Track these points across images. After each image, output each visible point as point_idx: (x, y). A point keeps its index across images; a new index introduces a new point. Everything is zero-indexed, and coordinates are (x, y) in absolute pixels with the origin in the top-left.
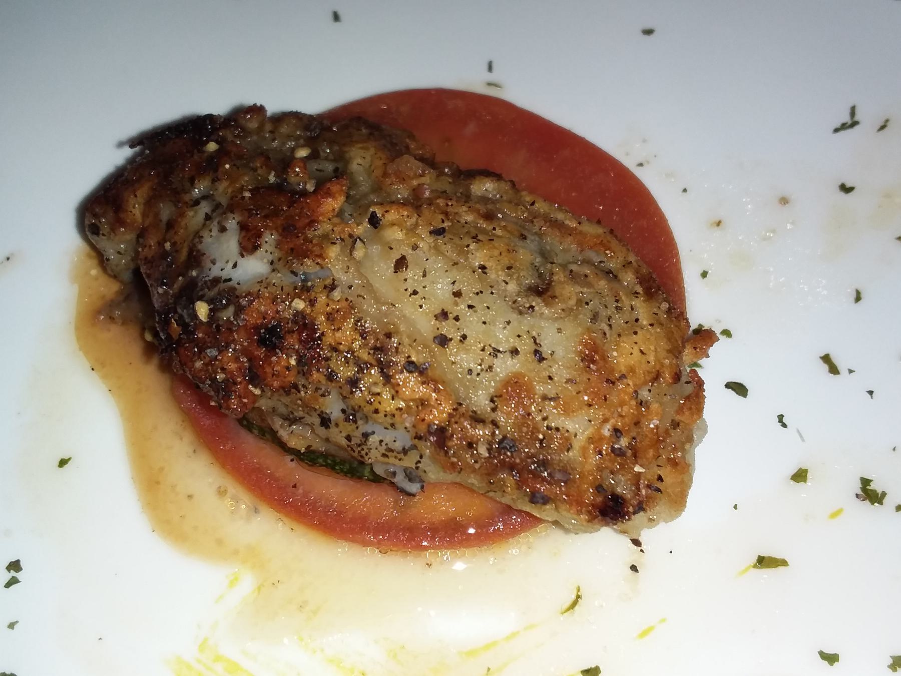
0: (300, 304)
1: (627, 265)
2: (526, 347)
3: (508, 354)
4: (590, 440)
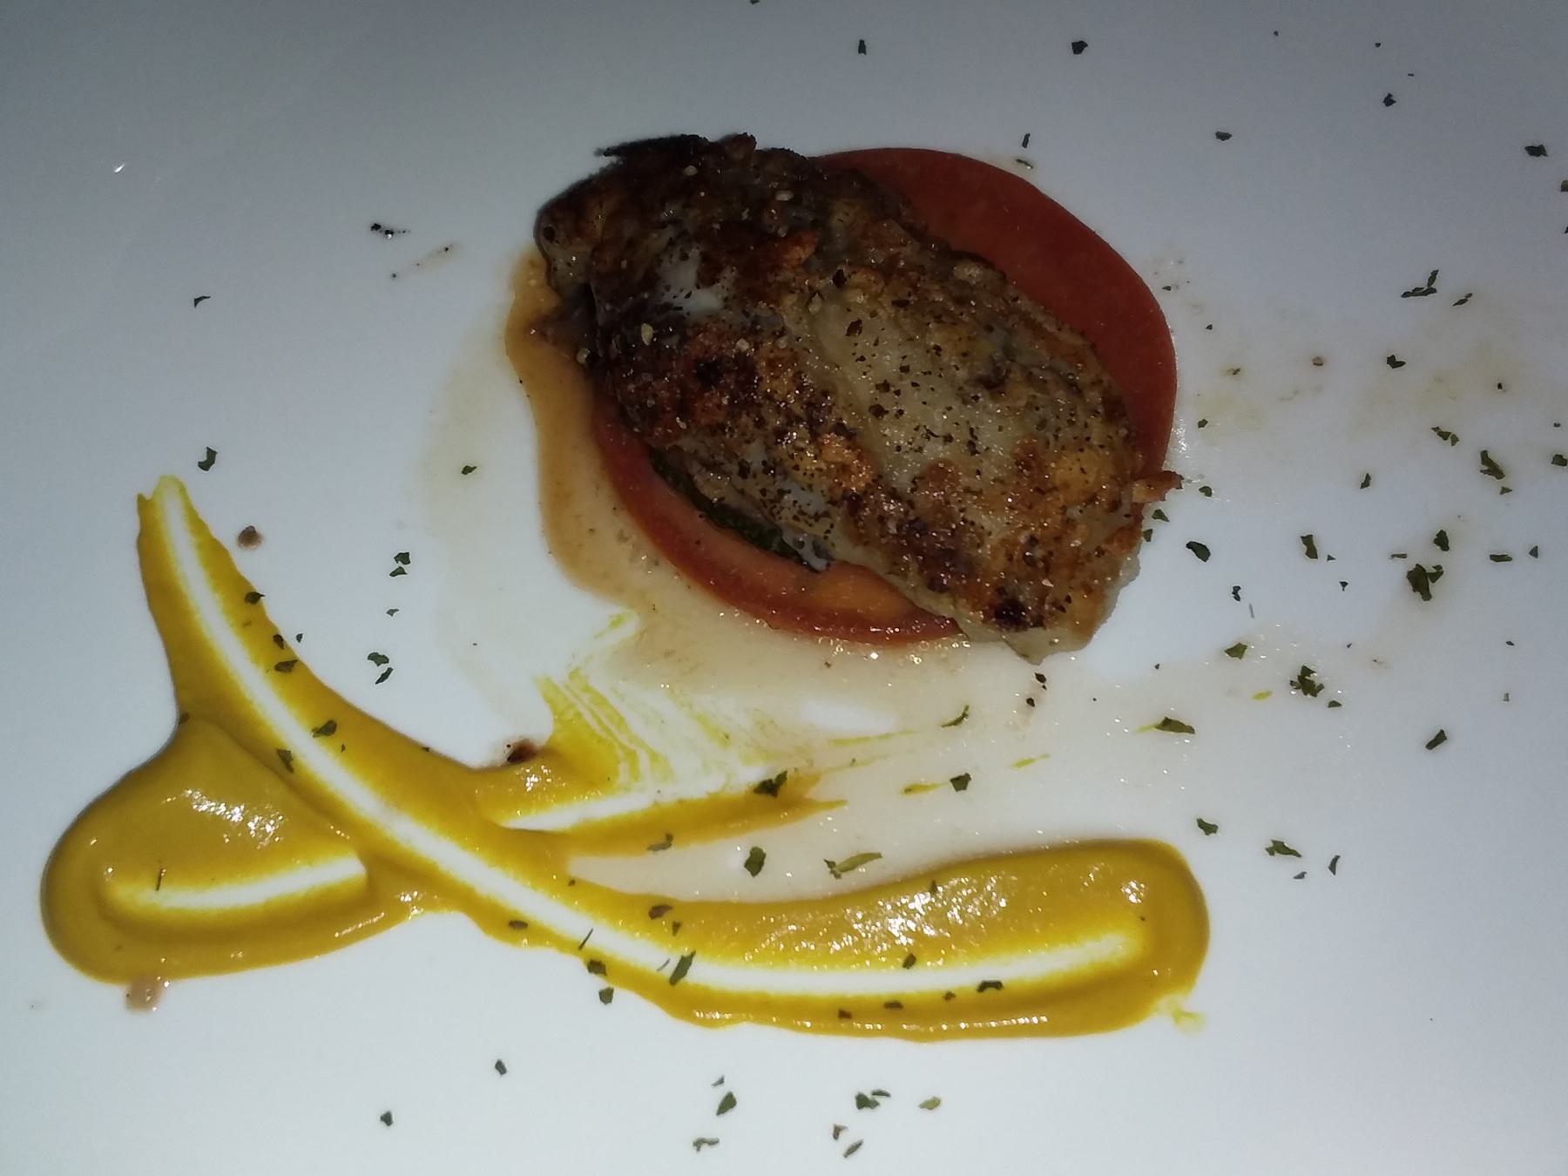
0: (743, 345)
1: (1097, 382)
2: (961, 437)
3: (941, 440)
4: (1004, 541)
